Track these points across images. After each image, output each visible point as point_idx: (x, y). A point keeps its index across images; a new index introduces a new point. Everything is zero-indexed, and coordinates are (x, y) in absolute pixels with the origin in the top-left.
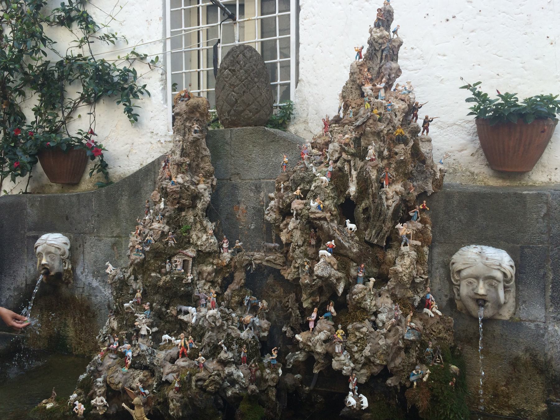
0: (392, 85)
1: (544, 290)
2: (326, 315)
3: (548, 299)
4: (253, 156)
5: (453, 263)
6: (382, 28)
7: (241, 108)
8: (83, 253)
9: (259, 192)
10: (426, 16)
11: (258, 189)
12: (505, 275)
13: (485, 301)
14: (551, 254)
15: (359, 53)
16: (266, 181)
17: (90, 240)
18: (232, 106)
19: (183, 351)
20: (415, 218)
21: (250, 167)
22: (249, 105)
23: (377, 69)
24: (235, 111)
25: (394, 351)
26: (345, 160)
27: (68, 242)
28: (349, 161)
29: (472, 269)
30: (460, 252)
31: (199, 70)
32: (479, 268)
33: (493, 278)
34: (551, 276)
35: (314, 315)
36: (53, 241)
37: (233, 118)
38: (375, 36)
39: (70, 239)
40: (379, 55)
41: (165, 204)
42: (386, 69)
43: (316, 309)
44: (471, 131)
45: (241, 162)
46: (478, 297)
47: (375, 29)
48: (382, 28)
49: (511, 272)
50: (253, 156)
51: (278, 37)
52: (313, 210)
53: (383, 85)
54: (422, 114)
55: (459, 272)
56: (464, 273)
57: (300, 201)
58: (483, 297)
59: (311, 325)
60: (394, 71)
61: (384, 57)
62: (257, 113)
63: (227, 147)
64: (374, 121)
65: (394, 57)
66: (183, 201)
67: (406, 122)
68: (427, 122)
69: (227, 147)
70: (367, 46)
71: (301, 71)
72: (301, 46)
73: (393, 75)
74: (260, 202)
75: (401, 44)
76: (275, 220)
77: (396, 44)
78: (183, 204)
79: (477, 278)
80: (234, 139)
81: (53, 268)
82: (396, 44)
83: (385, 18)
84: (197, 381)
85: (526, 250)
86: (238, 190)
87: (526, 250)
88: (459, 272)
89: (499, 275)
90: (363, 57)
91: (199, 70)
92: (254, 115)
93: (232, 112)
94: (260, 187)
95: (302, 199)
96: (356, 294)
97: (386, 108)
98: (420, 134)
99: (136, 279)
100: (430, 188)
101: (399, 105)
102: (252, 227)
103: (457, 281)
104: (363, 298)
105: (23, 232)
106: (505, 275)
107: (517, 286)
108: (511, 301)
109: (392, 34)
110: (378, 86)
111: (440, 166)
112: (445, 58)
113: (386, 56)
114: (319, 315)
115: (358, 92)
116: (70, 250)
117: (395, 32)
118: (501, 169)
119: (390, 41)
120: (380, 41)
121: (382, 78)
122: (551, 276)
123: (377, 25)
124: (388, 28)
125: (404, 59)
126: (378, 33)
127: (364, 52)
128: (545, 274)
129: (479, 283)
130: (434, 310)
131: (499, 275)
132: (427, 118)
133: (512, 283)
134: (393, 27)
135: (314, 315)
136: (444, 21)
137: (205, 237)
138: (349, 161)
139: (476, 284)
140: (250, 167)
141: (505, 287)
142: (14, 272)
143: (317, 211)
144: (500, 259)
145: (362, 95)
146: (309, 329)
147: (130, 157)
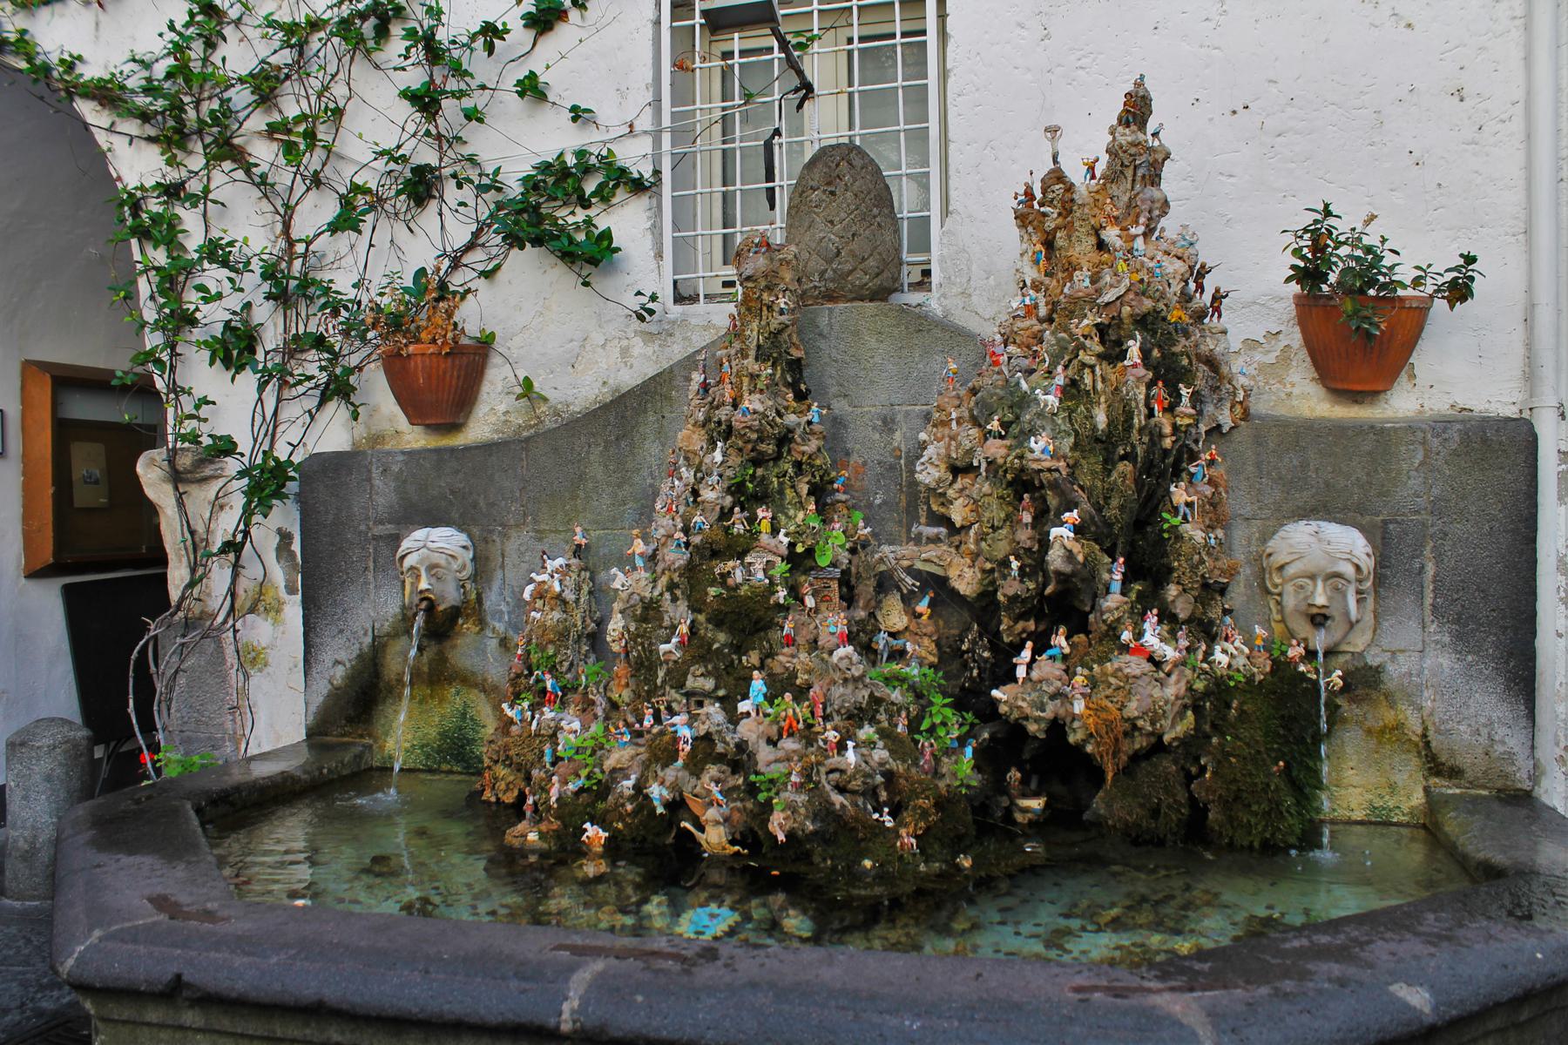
0: (1154, 229)
1: (1421, 596)
2: (1050, 652)
3: (1428, 611)
4: (878, 359)
5: (1270, 555)
6: (1133, 127)
7: (848, 267)
8: (503, 567)
9: (892, 431)
10: (1240, 109)
11: (888, 424)
12: (1358, 568)
13: (1326, 618)
14: (1432, 530)
15: (1091, 168)
16: (905, 408)
17: (516, 543)
18: (829, 261)
19: (791, 726)
20: (1200, 476)
21: (872, 382)
22: (864, 259)
23: (1126, 199)
24: (835, 271)
25: (1176, 709)
26: (1084, 365)
27: (469, 543)
28: (1092, 367)
29: (1305, 561)
30: (1281, 533)
31: (770, 185)
32: (1316, 560)
33: (1338, 575)
34: (1430, 569)
35: (1026, 654)
36: (436, 546)
37: (831, 285)
38: (1122, 140)
39: (470, 537)
40: (1129, 173)
41: (724, 454)
42: (1143, 201)
43: (1029, 644)
44: (1285, 317)
45: (852, 373)
46: (1315, 611)
47: (1120, 129)
48: (1133, 127)
49: (1368, 564)
50: (878, 359)
51: (902, 126)
52: (1037, 454)
53: (1141, 229)
54: (1210, 283)
55: (1281, 568)
56: (1290, 571)
57: (999, 442)
58: (1323, 611)
59: (1021, 672)
60: (1158, 205)
61: (1138, 178)
62: (878, 275)
63: (822, 344)
64: (1137, 294)
65: (1154, 179)
66: (763, 447)
67: (1186, 298)
68: (1218, 297)
69: (822, 344)
70: (1104, 158)
71: (952, 193)
72: (952, 147)
73: (1157, 212)
74: (894, 450)
75: (1167, 156)
76: (939, 481)
77: (1160, 157)
78: (760, 453)
79: (1313, 577)
80: (836, 327)
81: (443, 598)
82: (1160, 157)
83: (1137, 109)
84: (828, 773)
85: (1391, 527)
86: (845, 427)
87: (1391, 527)
88: (1281, 568)
89: (1348, 570)
90: (1098, 175)
91: (770, 185)
92: (871, 280)
93: (830, 274)
94: (893, 421)
95: (1001, 437)
96: (1110, 611)
97: (1150, 271)
98: (1206, 321)
99: (674, 599)
100: (1226, 419)
101: (1174, 267)
102: (878, 502)
103: (1276, 586)
104: (1119, 619)
105: (363, 527)
106: (1358, 568)
107: (1376, 592)
108: (1369, 618)
109: (1150, 138)
110: (1133, 231)
111: (1242, 380)
112: (1232, 180)
113: (1144, 177)
114: (1037, 652)
115: (1092, 240)
116: (474, 559)
117: (1155, 135)
118: (1339, 386)
119: (1151, 150)
120: (1133, 150)
121: (1138, 216)
122: (1430, 569)
123: (1124, 121)
124: (1142, 125)
125: (1171, 182)
126: (1126, 136)
127: (1100, 169)
128: (1423, 567)
129: (1315, 585)
130: (1237, 643)
131: (1348, 570)
132: (1217, 290)
133: (1369, 584)
134: (1151, 126)
135: (1026, 654)
136: (1228, 113)
137: (801, 515)
138: (1092, 367)
139: (1310, 588)
140: (872, 382)
141: (1359, 592)
142: (345, 611)
143: (1043, 457)
144: (1347, 544)
145: (1101, 246)
146: (1015, 680)
147: (579, 368)
